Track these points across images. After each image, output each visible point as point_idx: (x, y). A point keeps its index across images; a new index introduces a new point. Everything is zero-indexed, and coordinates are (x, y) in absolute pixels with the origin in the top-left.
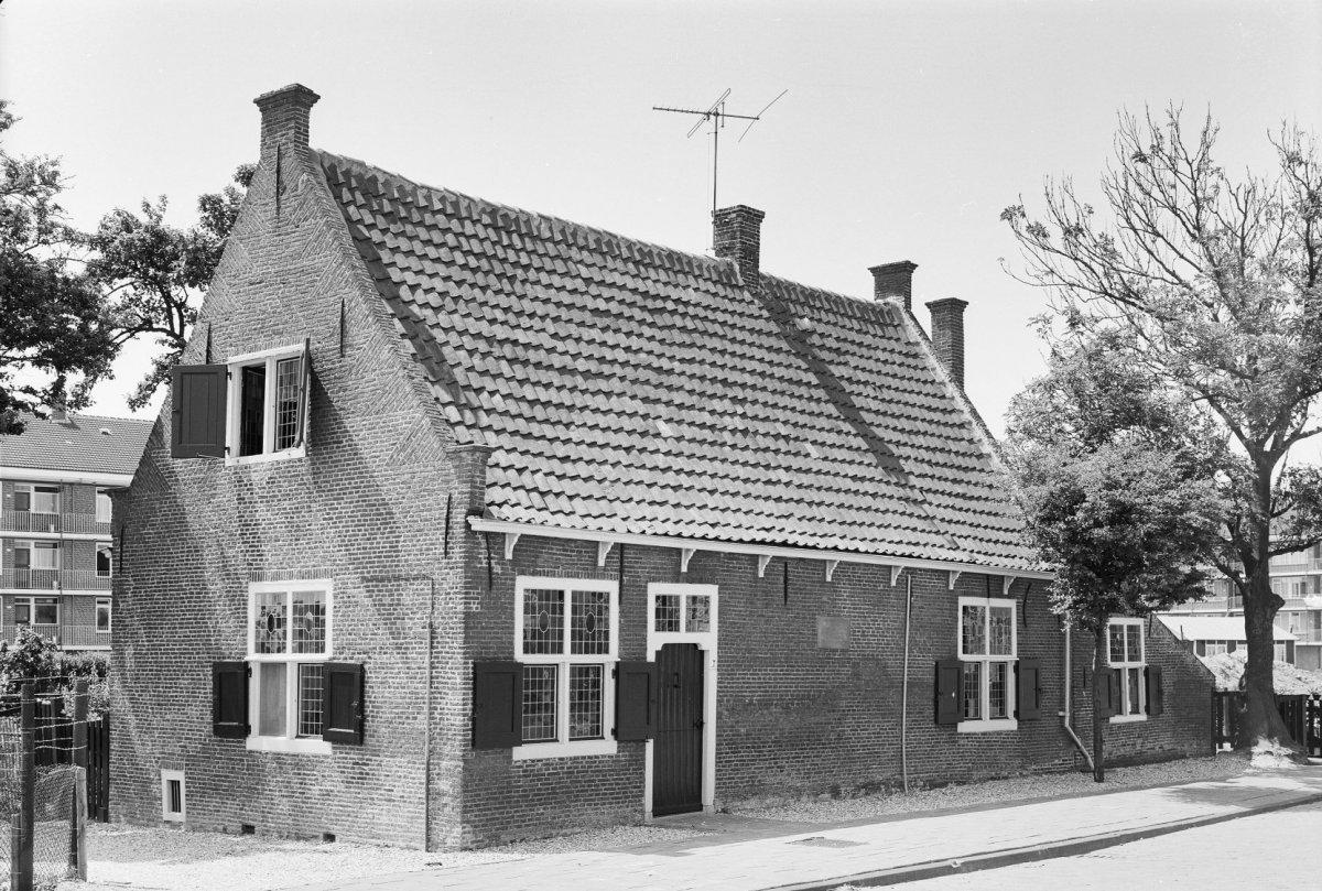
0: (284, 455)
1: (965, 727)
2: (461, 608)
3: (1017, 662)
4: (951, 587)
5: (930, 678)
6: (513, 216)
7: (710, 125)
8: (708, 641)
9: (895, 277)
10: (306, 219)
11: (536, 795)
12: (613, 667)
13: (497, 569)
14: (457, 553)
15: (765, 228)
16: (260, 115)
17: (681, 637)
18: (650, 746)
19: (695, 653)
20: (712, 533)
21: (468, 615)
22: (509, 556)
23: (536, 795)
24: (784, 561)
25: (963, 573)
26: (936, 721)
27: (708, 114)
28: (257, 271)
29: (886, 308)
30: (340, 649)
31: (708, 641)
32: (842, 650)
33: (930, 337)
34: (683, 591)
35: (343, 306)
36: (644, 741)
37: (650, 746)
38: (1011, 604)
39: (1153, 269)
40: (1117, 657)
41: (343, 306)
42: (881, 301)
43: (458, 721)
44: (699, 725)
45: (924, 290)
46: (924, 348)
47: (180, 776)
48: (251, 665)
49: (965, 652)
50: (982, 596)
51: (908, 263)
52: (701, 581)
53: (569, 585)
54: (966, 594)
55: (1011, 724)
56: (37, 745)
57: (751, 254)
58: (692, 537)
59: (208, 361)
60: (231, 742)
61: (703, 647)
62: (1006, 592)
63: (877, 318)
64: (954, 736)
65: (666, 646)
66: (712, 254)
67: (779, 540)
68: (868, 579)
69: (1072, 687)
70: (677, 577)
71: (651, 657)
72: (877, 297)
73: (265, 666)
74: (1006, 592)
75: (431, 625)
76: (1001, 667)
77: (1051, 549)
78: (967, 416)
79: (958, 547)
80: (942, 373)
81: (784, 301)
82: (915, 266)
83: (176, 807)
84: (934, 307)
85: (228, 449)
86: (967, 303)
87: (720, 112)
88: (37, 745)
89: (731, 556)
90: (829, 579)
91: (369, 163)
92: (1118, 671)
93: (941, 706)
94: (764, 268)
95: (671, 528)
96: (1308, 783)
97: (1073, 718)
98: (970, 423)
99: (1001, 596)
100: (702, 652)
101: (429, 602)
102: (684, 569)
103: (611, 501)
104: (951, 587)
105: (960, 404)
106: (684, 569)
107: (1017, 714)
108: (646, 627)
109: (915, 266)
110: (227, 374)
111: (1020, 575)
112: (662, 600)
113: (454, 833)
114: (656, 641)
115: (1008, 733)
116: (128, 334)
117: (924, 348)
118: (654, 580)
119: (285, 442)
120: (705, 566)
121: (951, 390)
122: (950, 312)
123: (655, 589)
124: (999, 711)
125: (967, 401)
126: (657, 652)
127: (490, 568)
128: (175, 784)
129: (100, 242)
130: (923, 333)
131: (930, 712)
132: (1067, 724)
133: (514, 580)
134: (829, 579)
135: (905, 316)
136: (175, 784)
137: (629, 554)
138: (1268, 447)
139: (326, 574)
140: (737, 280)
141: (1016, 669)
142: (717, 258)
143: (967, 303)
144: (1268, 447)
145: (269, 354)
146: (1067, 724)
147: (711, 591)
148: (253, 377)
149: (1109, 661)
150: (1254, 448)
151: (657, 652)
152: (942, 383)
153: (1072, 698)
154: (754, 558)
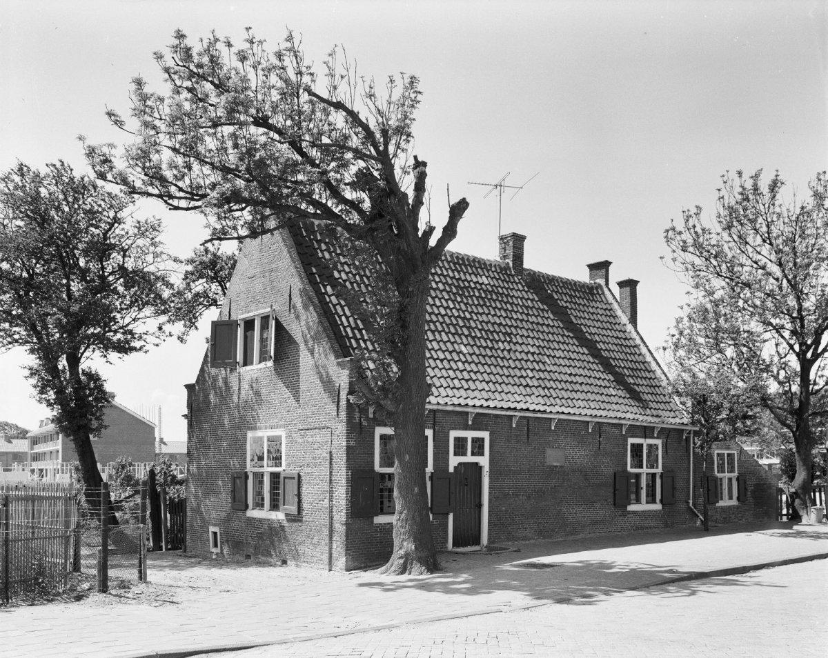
0: (262, 365)
1: (631, 508)
2: (345, 444)
3: (738, 477)
4: (624, 433)
5: (611, 481)
6: (460, 257)
7: (497, 191)
8: (484, 461)
9: (601, 267)
10: (274, 244)
11: (386, 542)
12: (430, 474)
13: (365, 423)
14: (343, 415)
15: (526, 244)
16: (637, 287)
17: (469, 458)
18: (451, 517)
19: (477, 468)
20: (485, 404)
21: (348, 448)
22: (371, 416)
23: (386, 542)
24: (528, 418)
25: (630, 425)
26: (615, 504)
27: (496, 186)
28: (252, 272)
29: (595, 286)
30: (289, 465)
31: (484, 461)
32: (561, 467)
33: (619, 300)
34: (470, 435)
35: (291, 288)
36: (448, 514)
37: (451, 517)
38: (659, 442)
39: (743, 259)
40: (721, 470)
41: (291, 288)
42: (592, 282)
43: (343, 502)
44: (479, 506)
45: (616, 275)
46: (615, 306)
47: (216, 529)
48: (248, 473)
49: (718, 472)
50: (642, 437)
51: (607, 261)
52: (479, 429)
53: (726, 452)
54: (632, 436)
55: (657, 507)
56: (109, 514)
57: (518, 258)
58: (574, 414)
59: (229, 318)
60: (240, 513)
61: (482, 464)
62: (656, 435)
63: (590, 292)
64: (626, 513)
65: (460, 464)
66: (498, 259)
67: (525, 408)
68: (576, 428)
69: (694, 487)
70: (466, 428)
71: (451, 470)
72: (591, 279)
73: (255, 474)
74: (656, 435)
75: (331, 452)
76: (654, 475)
77: (697, 416)
78: (638, 341)
79: (575, 406)
80: (624, 319)
81: (539, 284)
82: (611, 263)
83: (216, 545)
84: (622, 284)
85: (238, 363)
86: (639, 282)
87: (502, 184)
88: (109, 514)
89: (497, 416)
90: (553, 428)
91: (570, 278)
92: (638, 476)
93: (617, 496)
94: (526, 266)
95: (463, 402)
96: (512, 565)
97: (694, 504)
98: (639, 345)
99: (654, 438)
100: (481, 467)
101: (330, 440)
102: (470, 423)
103: (477, 389)
104: (624, 433)
105: (634, 335)
106: (470, 423)
107: (661, 501)
108: (448, 454)
109: (611, 263)
110: (238, 324)
111: (664, 426)
112: (457, 439)
113: (341, 561)
114: (454, 461)
115: (656, 511)
116: (205, 308)
117: (615, 306)
118: (453, 429)
119: (263, 359)
120: (481, 421)
121: (629, 327)
122: (630, 285)
123: (454, 434)
124: (651, 498)
125: (638, 333)
126: (455, 467)
127: (361, 423)
128: (215, 534)
129: (191, 261)
130: (615, 298)
131: (611, 500)
132: (691, 505)
133: (374, 429)
134: (553, 428)
135: (606, 290)
136: (215, 534)
137: (439, 415)
138: (809, 355)
139: (282, 426)
140: (511, 272)
141: (661, 476)
142: (501, 261)
143: (639, 282)
144: (809, 355)
145: (256, 312)
146: (691, 505)
147: (485, 435)
148: (249, 324)
149: (716, 473)
150: (801, 356)
151: (455, 467)
152: (625, 325)
153: (694, 492)
154: (510, 417)
